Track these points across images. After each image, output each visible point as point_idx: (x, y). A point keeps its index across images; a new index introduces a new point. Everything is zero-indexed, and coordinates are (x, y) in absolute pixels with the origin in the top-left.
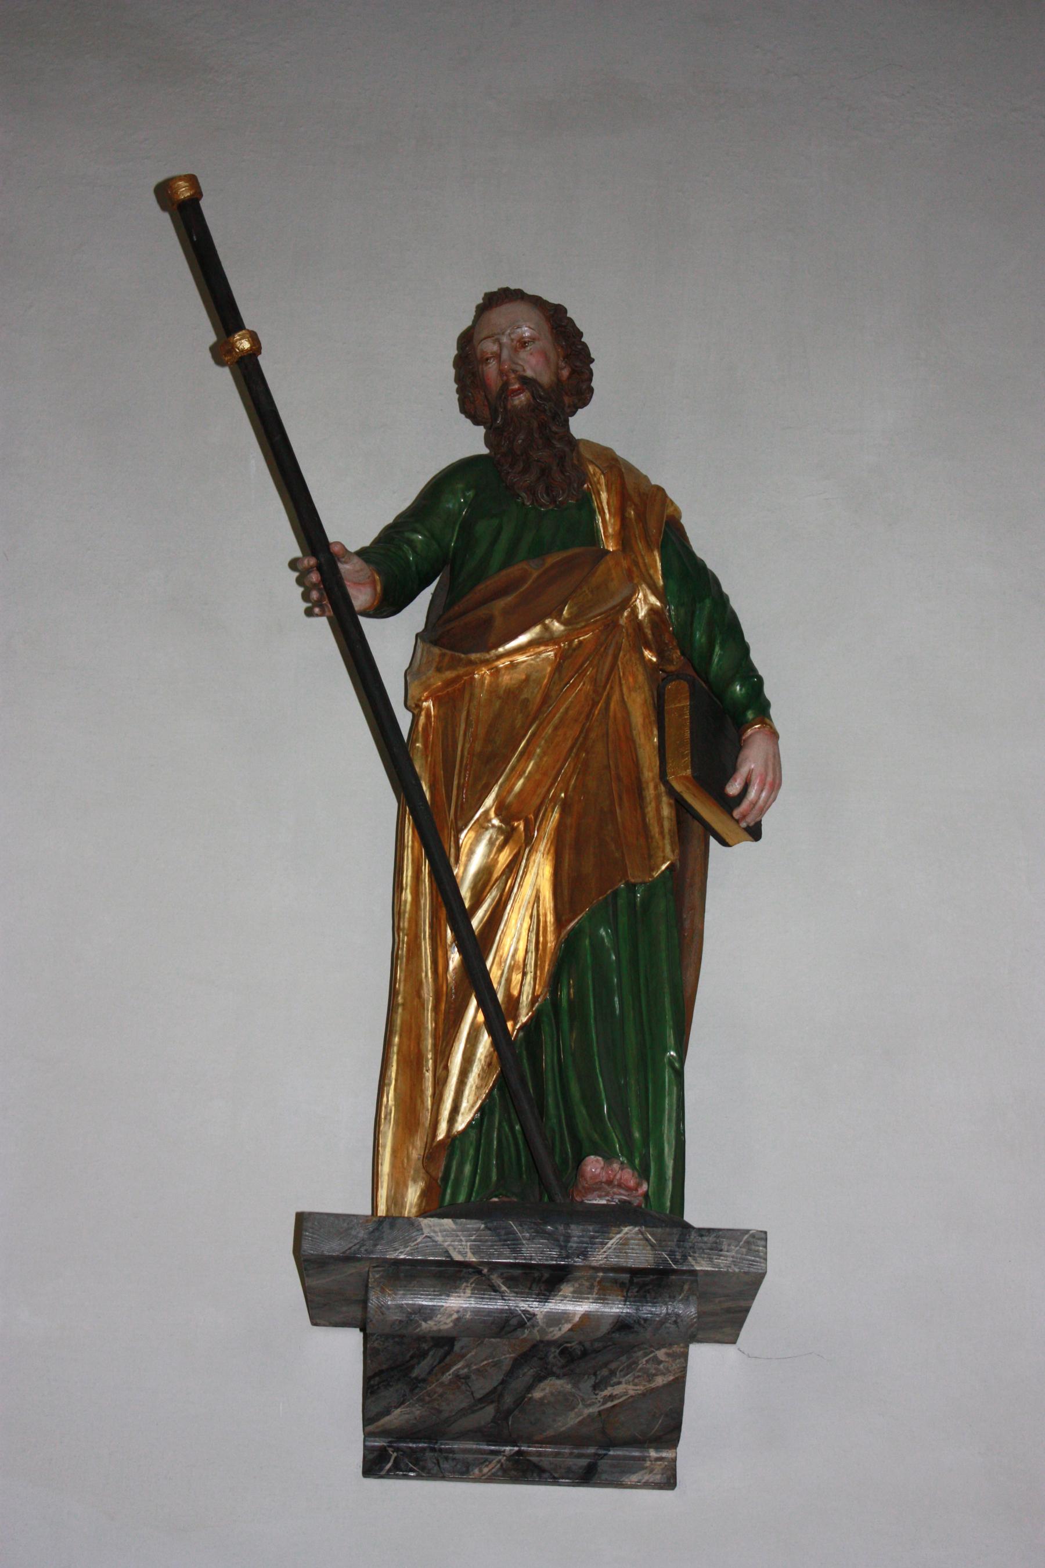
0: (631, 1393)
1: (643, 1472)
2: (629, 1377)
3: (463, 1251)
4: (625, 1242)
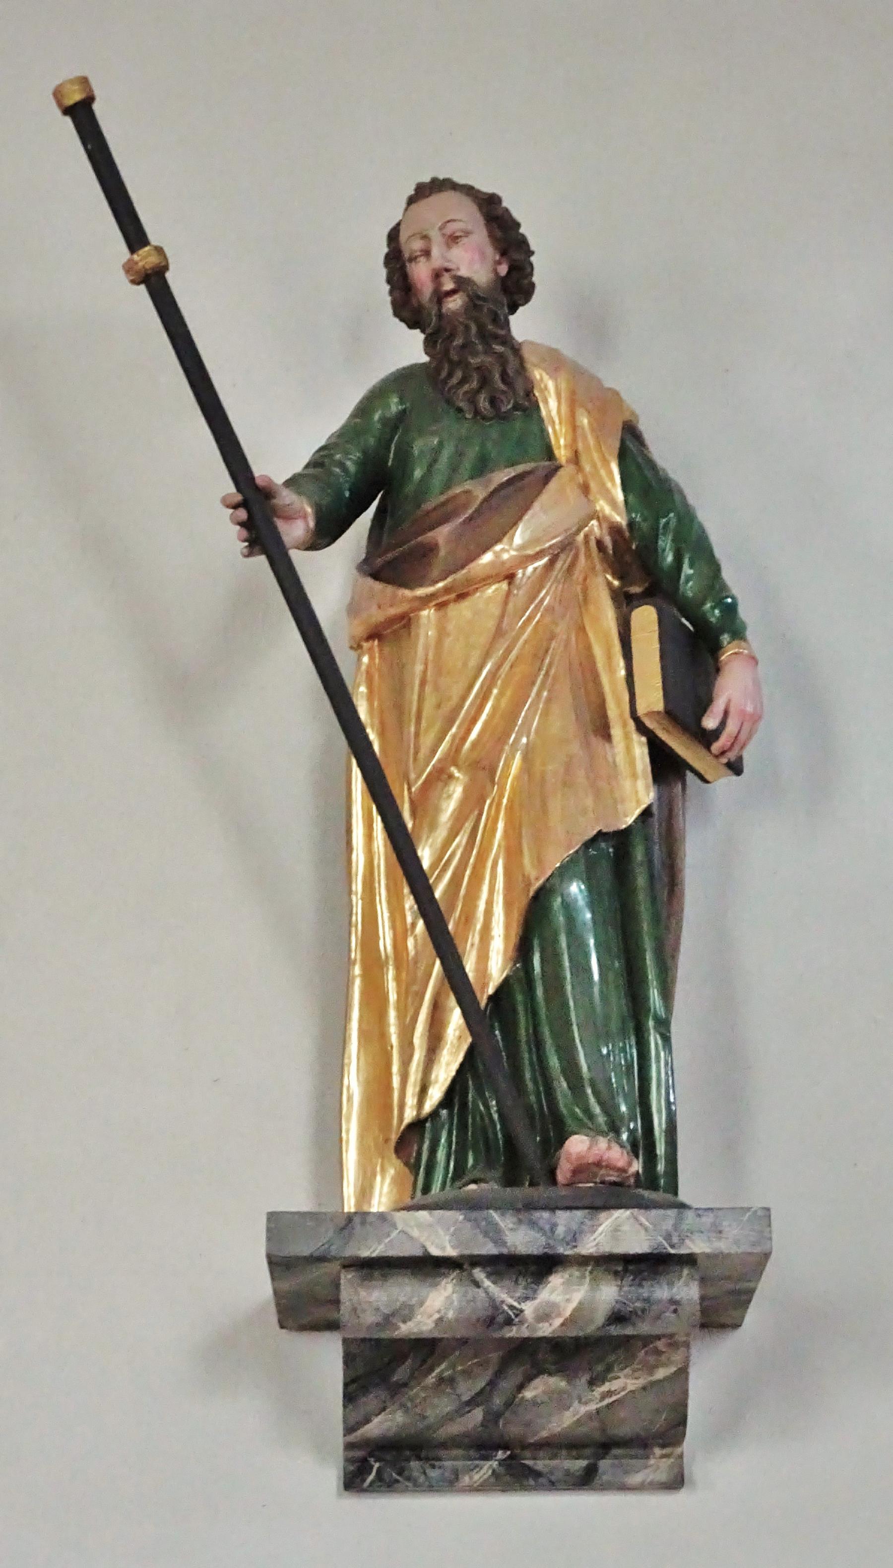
0: (630, 1388)
1: (647, 1471)
2: (628, 1371)
3: (442, 1246)
4: (616, 1229)
